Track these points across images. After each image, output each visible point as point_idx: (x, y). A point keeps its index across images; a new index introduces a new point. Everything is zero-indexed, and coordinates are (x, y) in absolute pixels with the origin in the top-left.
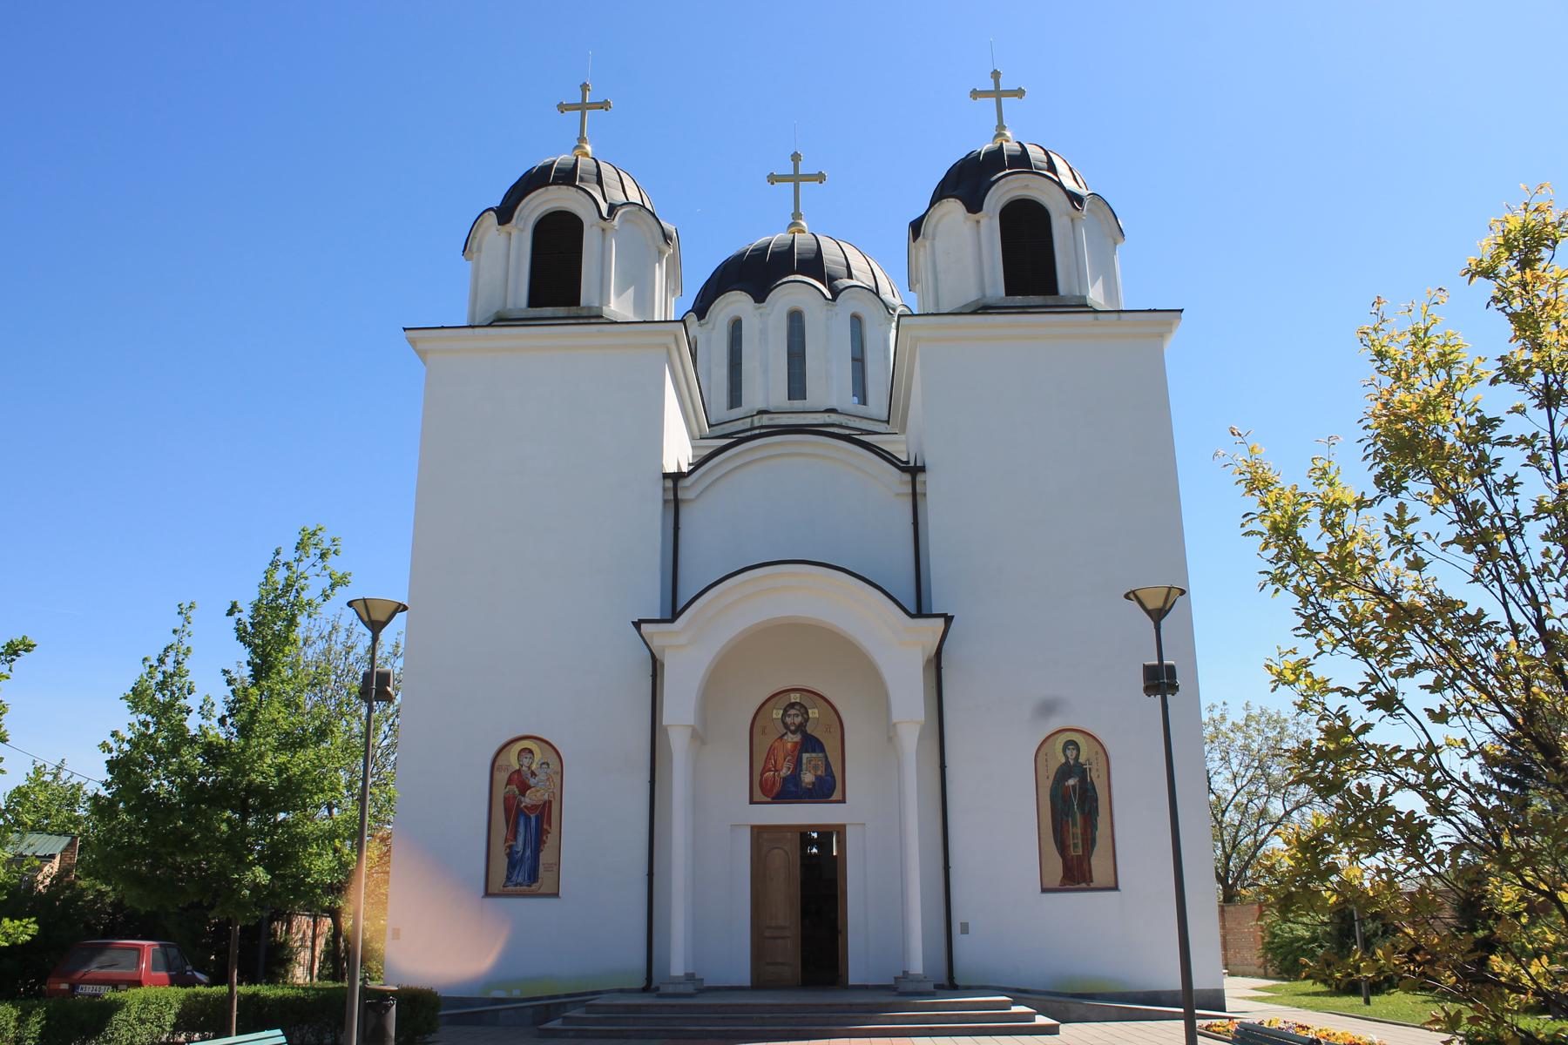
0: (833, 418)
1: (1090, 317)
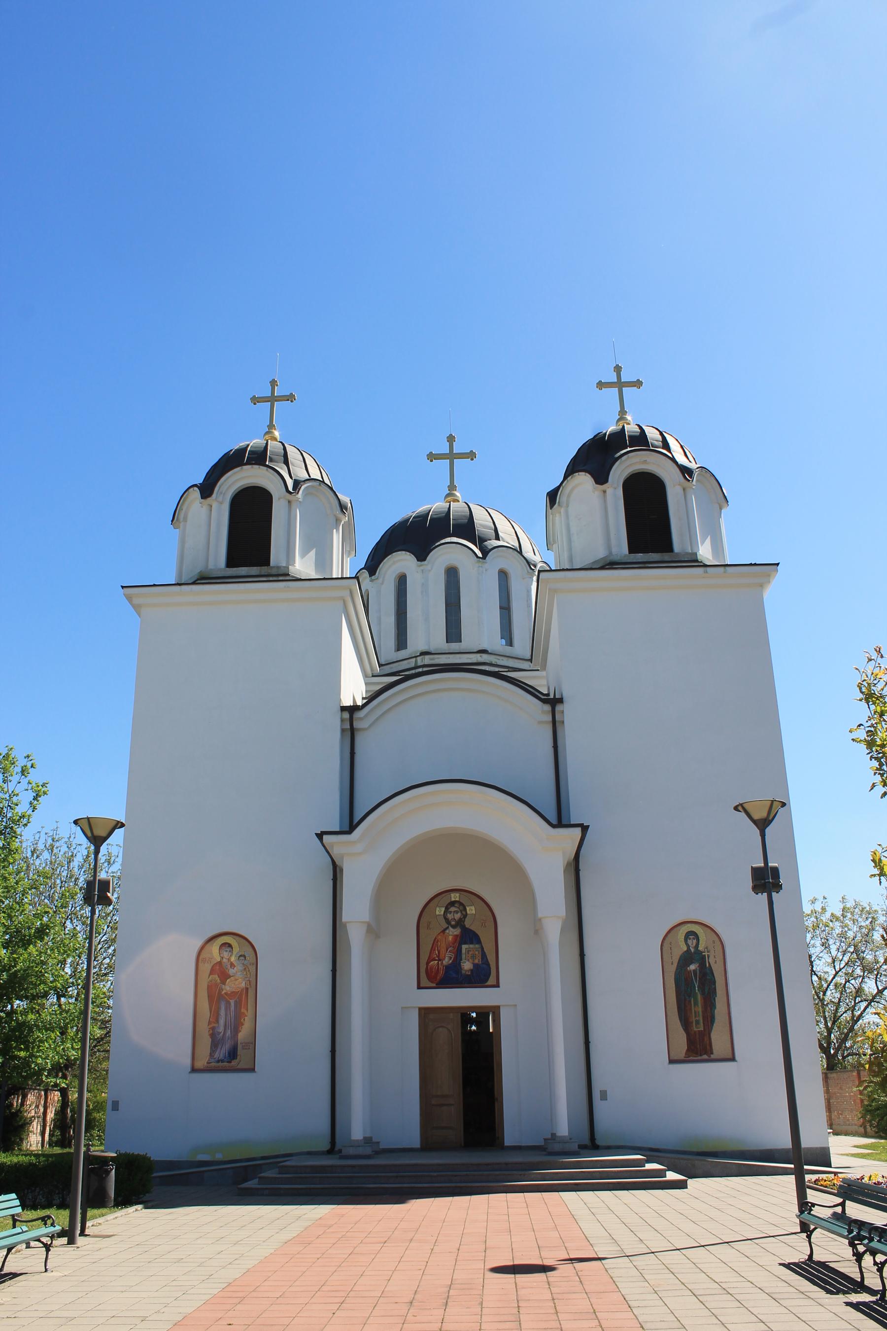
0: (485, 658)
1: (701, 570)
